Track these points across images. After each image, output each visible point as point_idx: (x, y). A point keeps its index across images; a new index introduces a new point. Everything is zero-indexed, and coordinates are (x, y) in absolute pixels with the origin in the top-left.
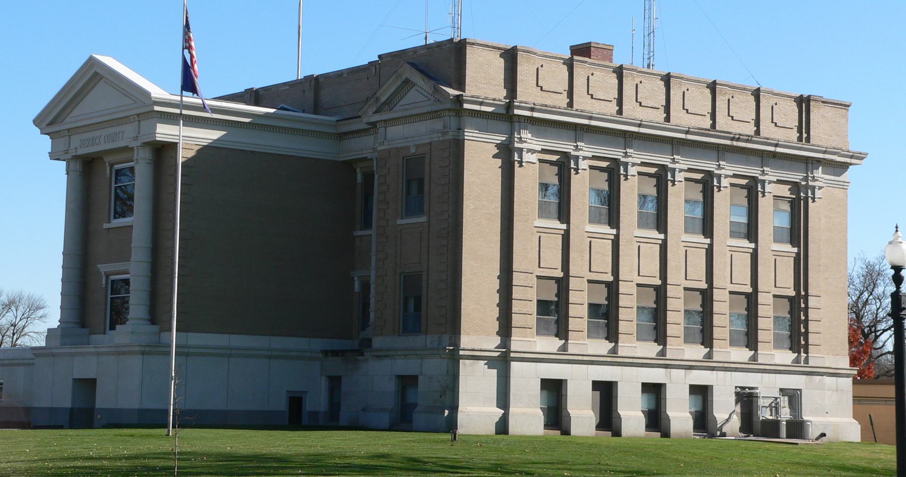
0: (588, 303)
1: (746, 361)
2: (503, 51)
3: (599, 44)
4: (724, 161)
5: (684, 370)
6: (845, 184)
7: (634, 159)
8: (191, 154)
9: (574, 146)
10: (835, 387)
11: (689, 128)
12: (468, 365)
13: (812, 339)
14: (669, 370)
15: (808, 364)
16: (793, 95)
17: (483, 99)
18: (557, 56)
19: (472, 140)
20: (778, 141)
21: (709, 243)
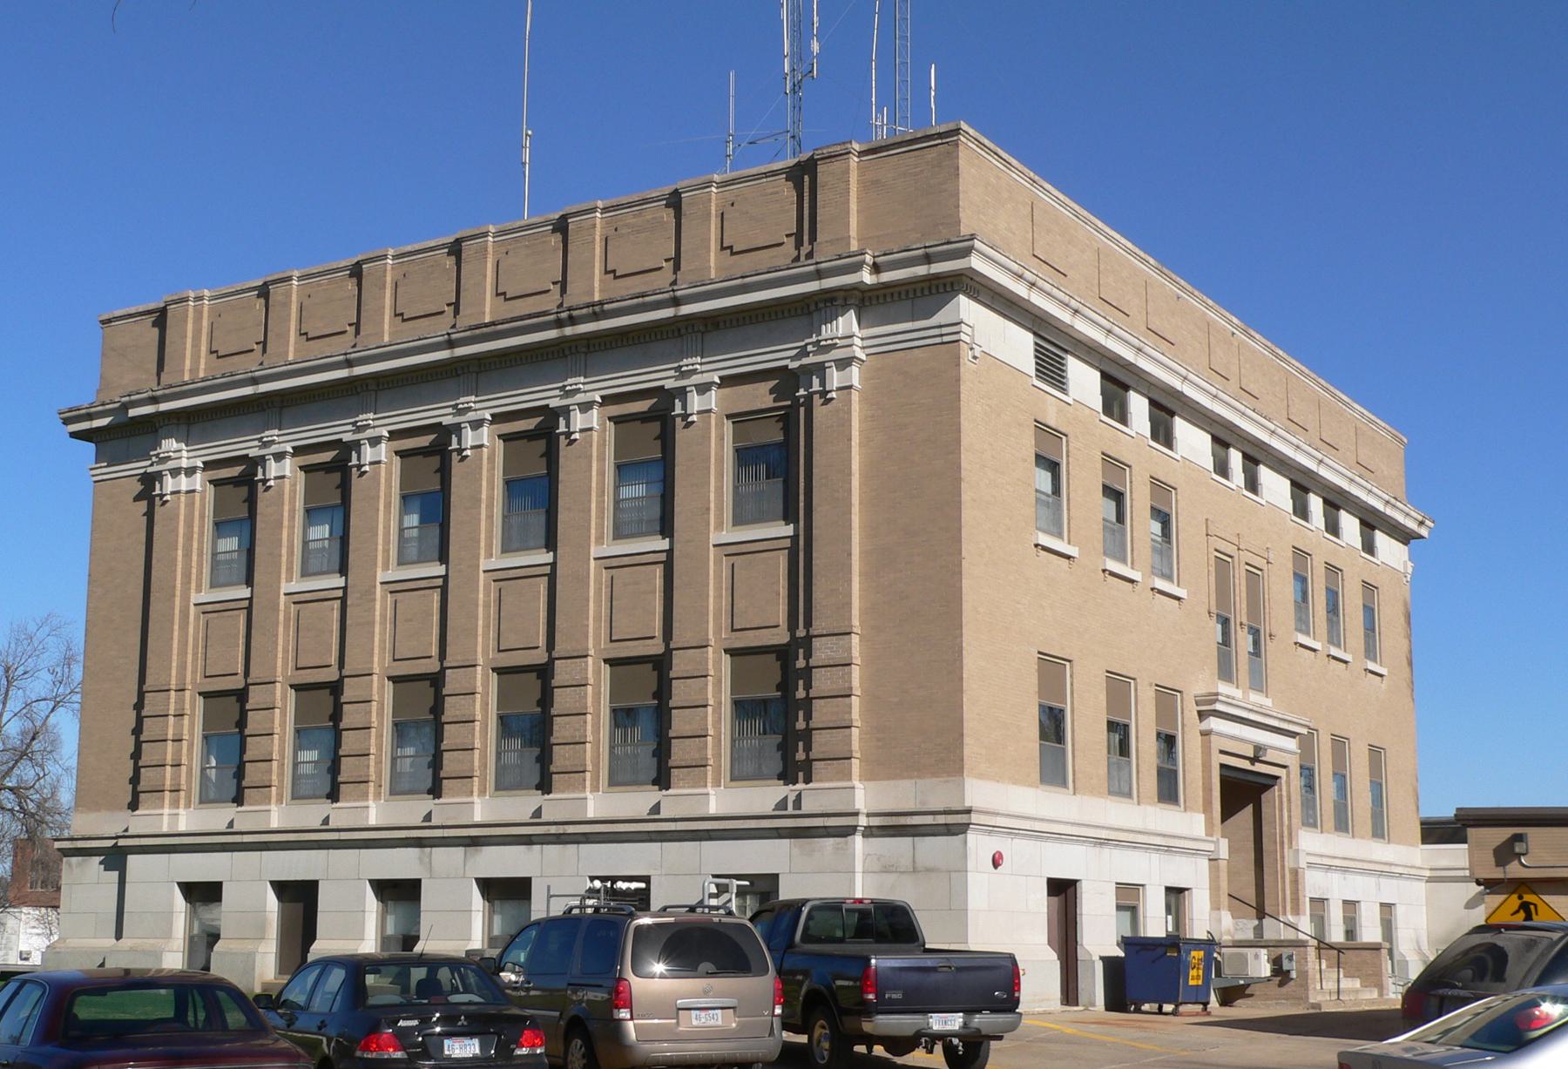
2: (158, 314)
4: (580, 376)
5: (461, 849)
7: (376, 429)
10: (911, 867)
12: (74, 866)
14: (427, 850)
15: (800, 809)
17: (87, 408)
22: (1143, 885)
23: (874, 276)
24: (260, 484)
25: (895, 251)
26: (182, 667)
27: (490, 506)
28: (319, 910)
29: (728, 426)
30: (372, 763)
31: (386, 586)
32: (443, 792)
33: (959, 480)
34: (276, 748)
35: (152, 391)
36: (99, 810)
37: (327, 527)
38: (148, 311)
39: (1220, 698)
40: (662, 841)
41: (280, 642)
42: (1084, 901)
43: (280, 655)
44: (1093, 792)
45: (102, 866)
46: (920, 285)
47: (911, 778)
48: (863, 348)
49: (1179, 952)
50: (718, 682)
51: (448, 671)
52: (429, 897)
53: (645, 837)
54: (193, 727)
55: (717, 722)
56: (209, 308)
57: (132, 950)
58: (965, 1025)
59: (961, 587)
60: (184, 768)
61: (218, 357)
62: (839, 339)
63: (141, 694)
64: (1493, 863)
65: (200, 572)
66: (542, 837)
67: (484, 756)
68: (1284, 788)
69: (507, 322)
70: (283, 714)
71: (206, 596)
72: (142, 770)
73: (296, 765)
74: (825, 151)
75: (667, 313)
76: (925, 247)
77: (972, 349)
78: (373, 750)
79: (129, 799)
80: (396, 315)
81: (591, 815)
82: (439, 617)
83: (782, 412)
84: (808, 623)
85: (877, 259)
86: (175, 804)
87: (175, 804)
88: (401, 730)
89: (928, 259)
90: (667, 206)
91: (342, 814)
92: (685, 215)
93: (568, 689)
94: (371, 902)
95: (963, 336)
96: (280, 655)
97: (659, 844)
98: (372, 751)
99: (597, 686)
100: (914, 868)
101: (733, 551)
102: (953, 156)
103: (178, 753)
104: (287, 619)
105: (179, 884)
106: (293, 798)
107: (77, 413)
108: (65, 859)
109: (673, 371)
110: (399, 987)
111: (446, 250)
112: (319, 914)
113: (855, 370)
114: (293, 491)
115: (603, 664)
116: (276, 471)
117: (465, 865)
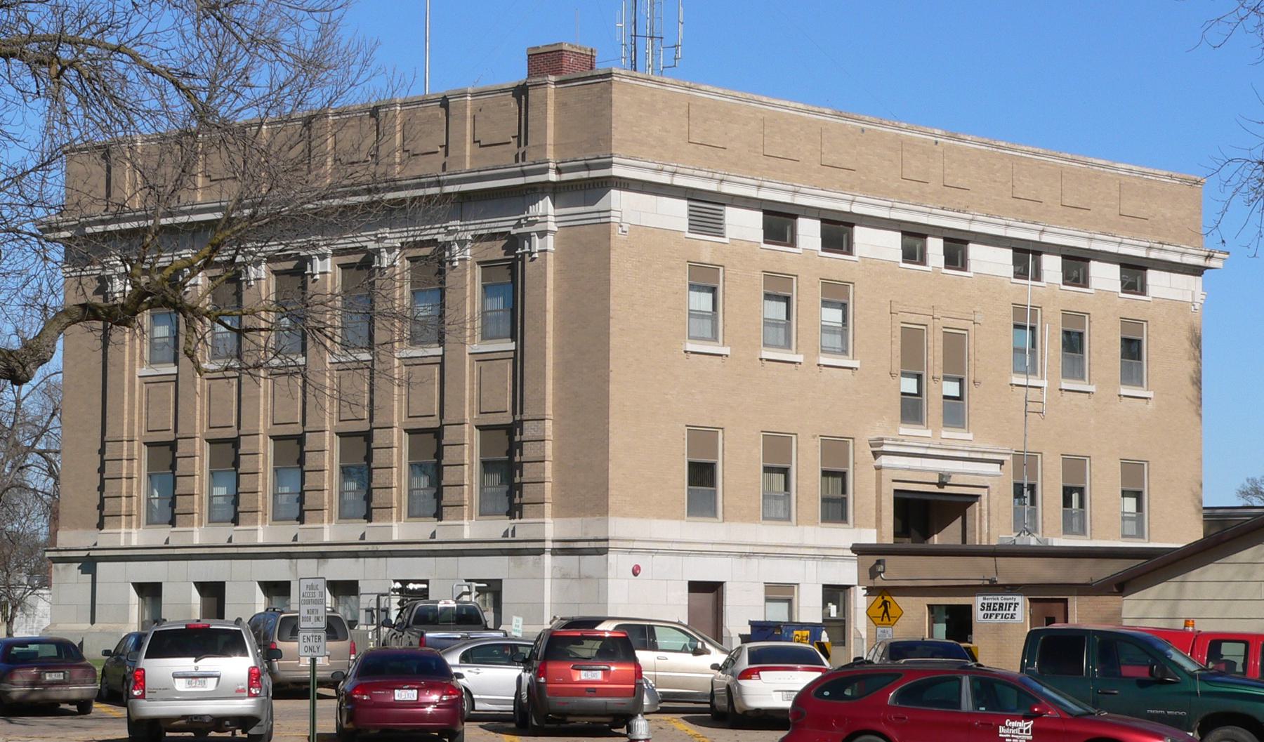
3: (538, 48)
5: (315, 560)
6: (602, 215)
10: (577, 574)
14: (294, 561)
22: (798, 584)
24: (309, 277)
26: (131, 423)
29: (478, 269)
30: (260, 498)
33: (608, 318)
34: (197, 485)
36: (77, 529)
40: (435, 556)
41: (198, 407)
42: (727, 596)
43: (198, 417)
44: (811, 522)
45: (80, 571)
48: (556, 222)
49: (781, 631)
50: (471, 448)
51: (307, 434)
53: (426, 553)
54: (140, 468)
55: (471, 475)
57: (101, 631)
60: (135, 499)
61: (481, 146)
63: (103, 443)
64: (869, 577)
67: (331, 495)
70: (202, 461)
71: (146, 371)
72: (106, 500)
73: (211, 497)
77: (621, 226)
78: (260, 489)
79: (98, 521)
80: (475, 142)
81: (395, 538)
84: (522, 412)
86: (129, 525)
87: (129, 525)
88: (346, 472)
89: (588, 167)
91: (374, 531)
93: (382, 450)
94: (134, 596)
95: (612, 219)
96: (198, 417)
98: (465, 483)
99: (400, 448)
101: (481, 358)
102: (608, 90)
103: (130, 487)
105: (133, 584)
106: (210, 522)
108: (53, 565)
113: (550, 239)
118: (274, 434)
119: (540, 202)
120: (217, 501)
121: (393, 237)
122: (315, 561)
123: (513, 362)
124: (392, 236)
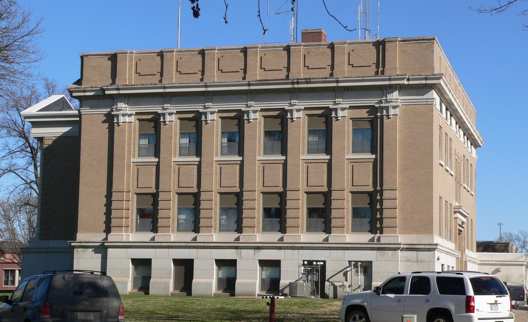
0: (137, 209)
1: (321, 242)
3: (308, 30)
8: (50, 142)
9: (245, 105)
10: (416, 259)
11: (249, 82)
12: (80, 252)
13: (386, 222)
14: (239, 250)
15: (380, 242)
16: (108, 53)
18: (151, 52)
19: (87, 114)
20: (337, 78)
21: (285, 159)
23: (407, 82)
25: (416, 75)
26: (128, 184)
27: (260, 139)
28: (194, 269)
31: (217, 162)
32: (243, 231)
35: (118, 86)
36: (90, 232)
37: (188, 139)
38: (106, 54)
39: (462, 208)
40: (330, 250)
46: (422, 85)
47: (415, 234)
52: (239, 265)
56: (134, 57)
58: (515, 303)
59: (433, 178)
62: (394, 99)
65: (134, 151)
66: (251, 247)
68: (463, 234)
69: (273, 81)
70: (174, 202)
73: (178, 220)
74: (389, 39)
75: (334, 85)
76: (426, 75)
82: (239, 174)
83: (370, 119)
84: (381, 185)
85: (409, 77)
86: (127, 231)
89: (426, 79)
90: (328, 48)
91: (160, 237)
92: (336, 52)
93: (292, 201)
95: (434, 103)
97: (329, 251)
100: (417, 260)
104: (174, 170)
107: (79, 89)
109: (332, 102)
110: (229, 294)
111: (240, 50)
112: (194, 270)
114: (176, 126)
115: (304, 193)
116: (169, 119)
117: (254, 255)
118: (307, 191)
119: (394, 93)
120: (181, 221)
121: (171, 108)
122: (253, 250)
123: (240, 166)
124: (344, 103)
